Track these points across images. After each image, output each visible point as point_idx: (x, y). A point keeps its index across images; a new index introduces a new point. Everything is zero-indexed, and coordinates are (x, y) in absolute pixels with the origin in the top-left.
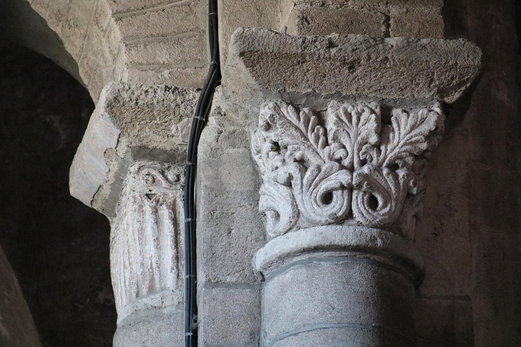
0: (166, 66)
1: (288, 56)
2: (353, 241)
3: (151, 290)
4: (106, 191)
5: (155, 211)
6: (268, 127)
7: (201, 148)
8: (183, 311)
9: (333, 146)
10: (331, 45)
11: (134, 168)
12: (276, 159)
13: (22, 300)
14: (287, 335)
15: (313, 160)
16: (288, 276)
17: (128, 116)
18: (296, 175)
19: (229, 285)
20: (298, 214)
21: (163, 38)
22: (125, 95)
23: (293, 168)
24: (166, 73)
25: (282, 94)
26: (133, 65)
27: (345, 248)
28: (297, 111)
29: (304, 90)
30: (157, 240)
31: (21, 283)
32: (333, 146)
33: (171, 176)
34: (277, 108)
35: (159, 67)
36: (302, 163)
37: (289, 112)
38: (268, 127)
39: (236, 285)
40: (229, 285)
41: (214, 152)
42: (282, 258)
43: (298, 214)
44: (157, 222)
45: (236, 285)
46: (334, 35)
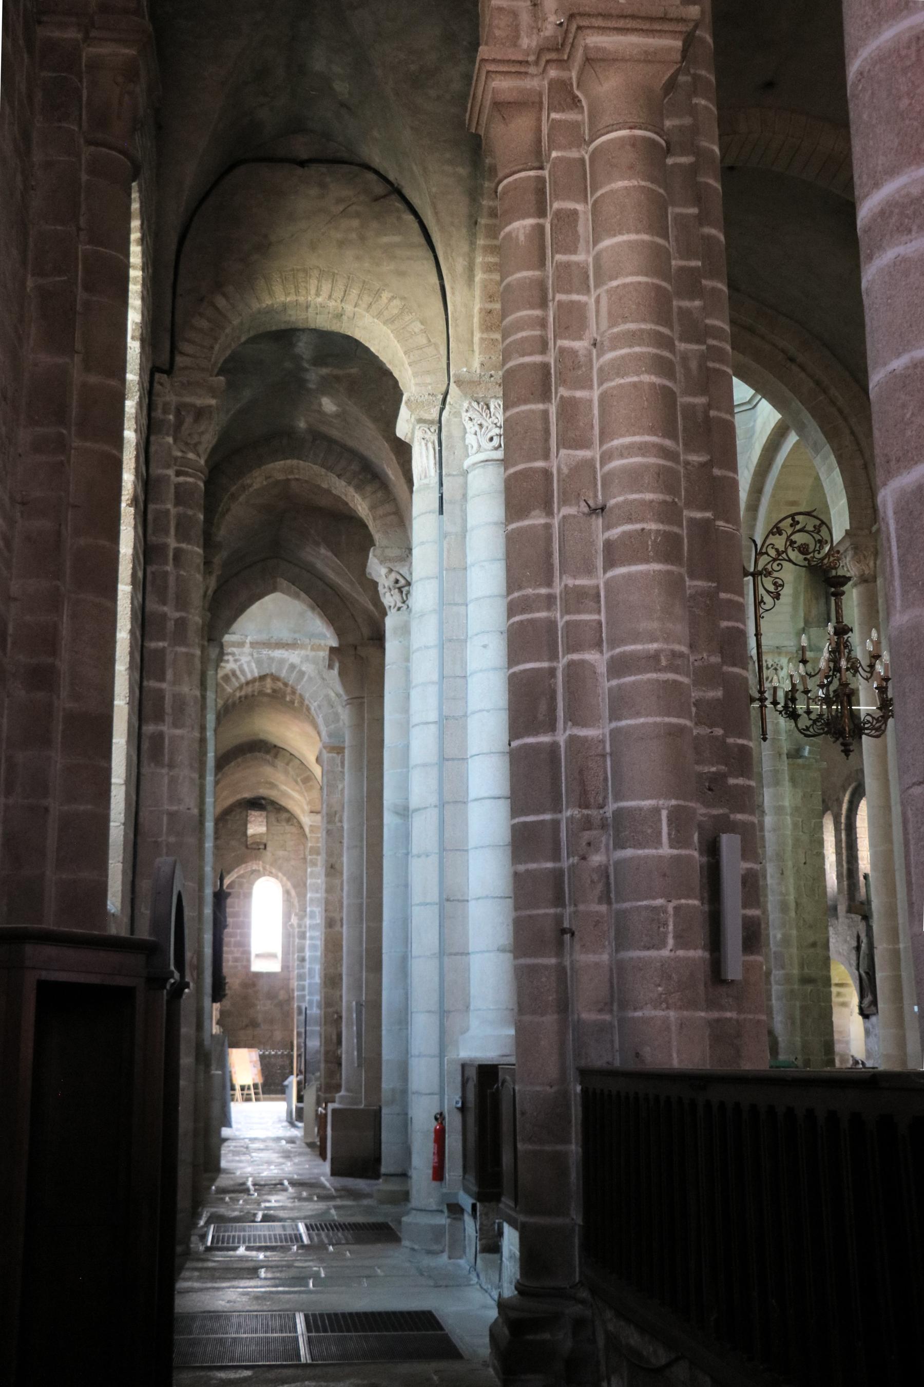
0: (430, 384)
1: (474, 382)
2: (903, 265)
3: (426, 477)
4: (409, 435)
5: (426, 445)
6: (467, 411)
7: (443, 419)
8: (437, 486)
9: (493, 418)
10: (491, 376)
11: (417, 427)
12: (470, 424)
13: (397, 466)
14: (419, 516)
15: (485, 424)
16: (476, 472)
17: (413, 406)
18: (478, 431)
19: (454, 476)
20: (480, 446)
21: (428, 372)
22: (412, 398)
23: (477, 428)
24: (430, 387)
25: (472, 397)
26: (417, 384)
27: (498, 460)
28: (478, 403)
29: (481, 395)
30: (427, 457)
31: (397, 459)
32: (493, 418)
33: (432, 430)
34: (470, 403)
35: (426, 385)
36: (481, 425)
37: (475, 404)
38: (467, 411)
39: (457, 475)
40: (454, 476)
41: (448, 421)
42: (474, 464)
43: (480, 446)
44: (427, 449)
45: (457, 475)
46: (493, 372)
